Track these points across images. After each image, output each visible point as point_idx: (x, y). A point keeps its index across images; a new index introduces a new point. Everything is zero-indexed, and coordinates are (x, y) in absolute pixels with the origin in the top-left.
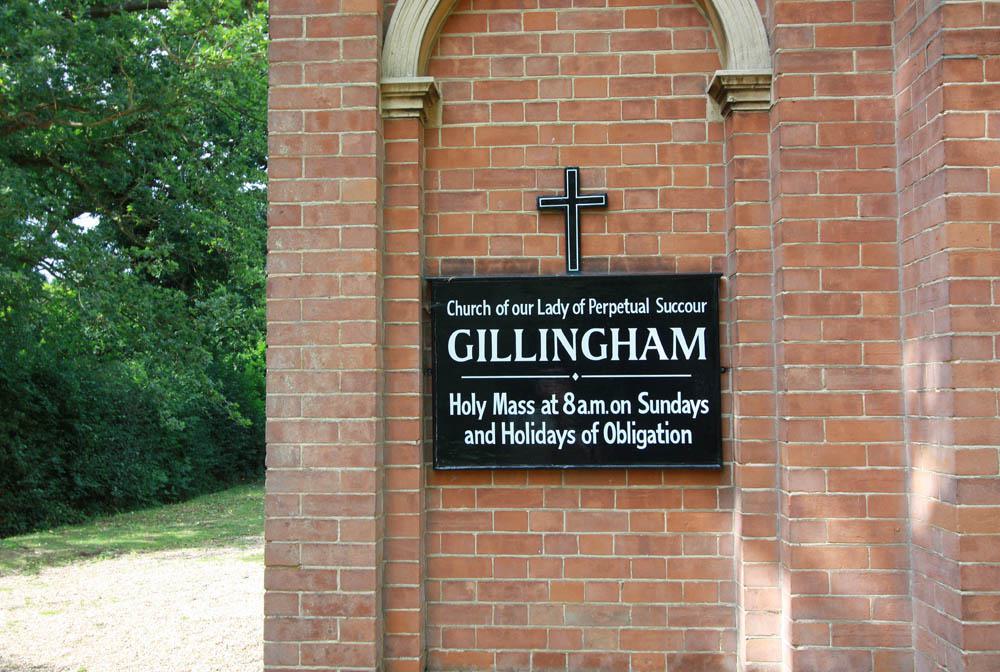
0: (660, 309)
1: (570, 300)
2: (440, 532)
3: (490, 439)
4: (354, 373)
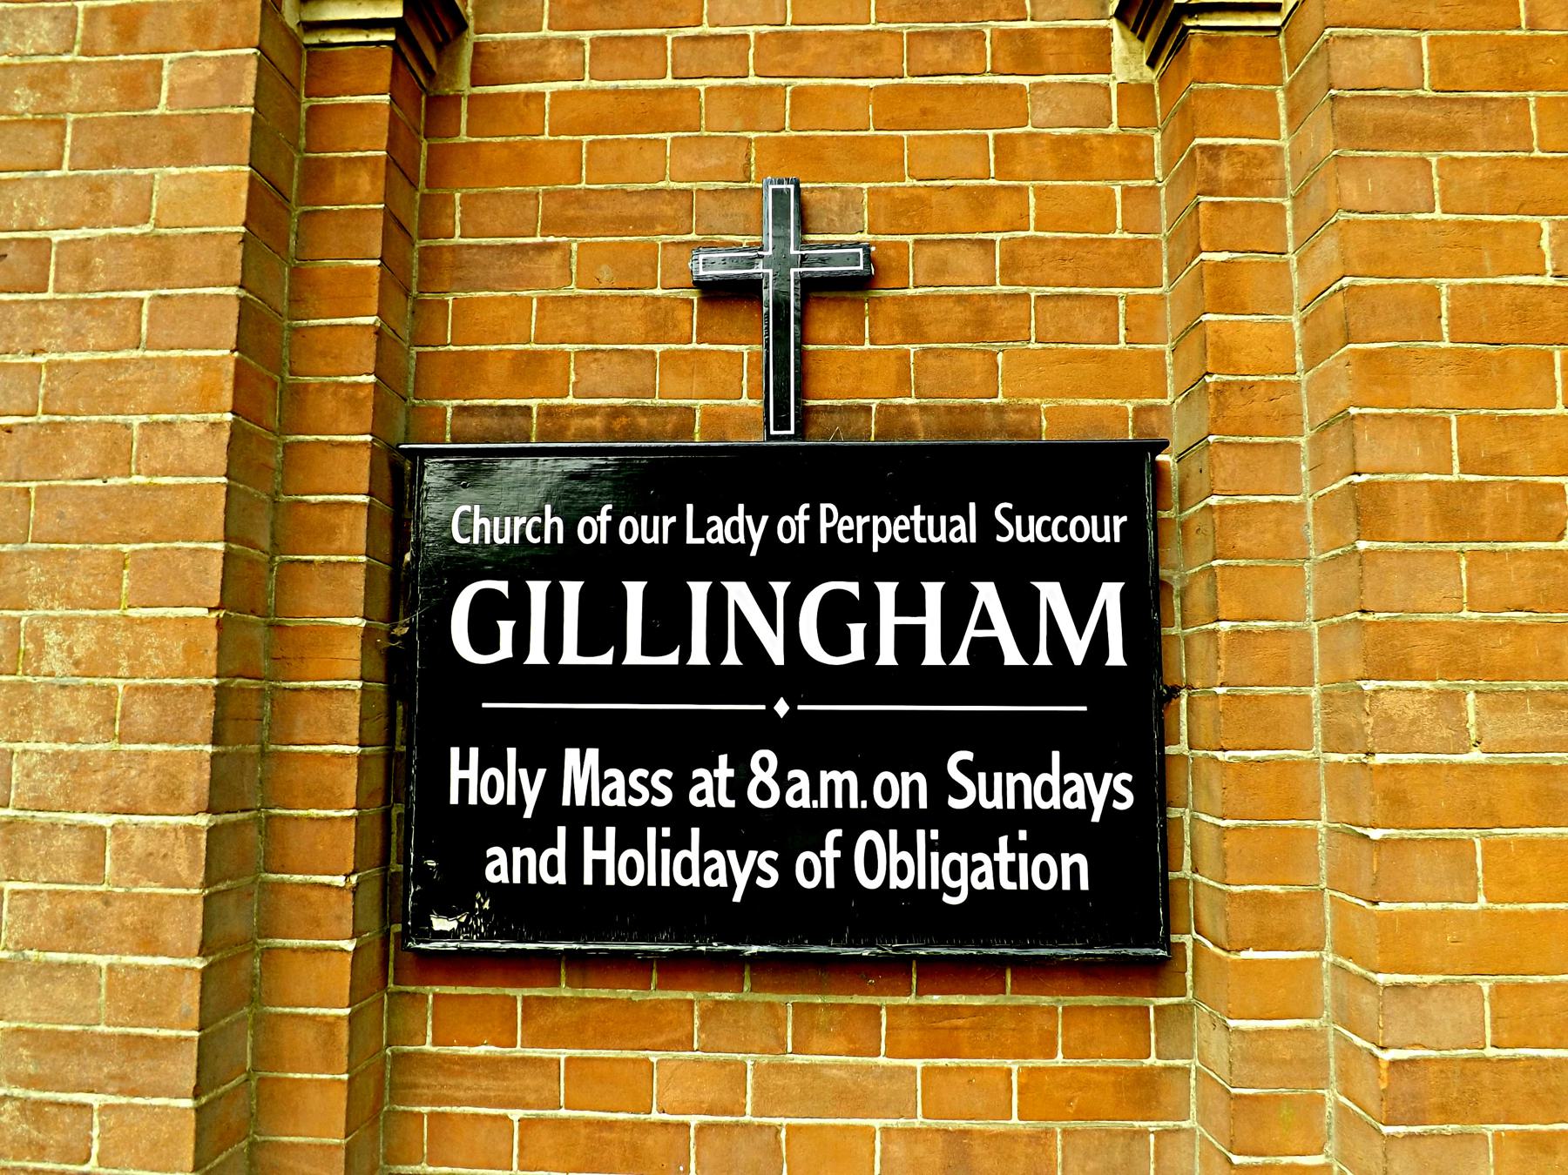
0: (1005, 532)
1: (771, 505)
2: (425, 1110)
3: (553, 870)
4: (157, 688)
